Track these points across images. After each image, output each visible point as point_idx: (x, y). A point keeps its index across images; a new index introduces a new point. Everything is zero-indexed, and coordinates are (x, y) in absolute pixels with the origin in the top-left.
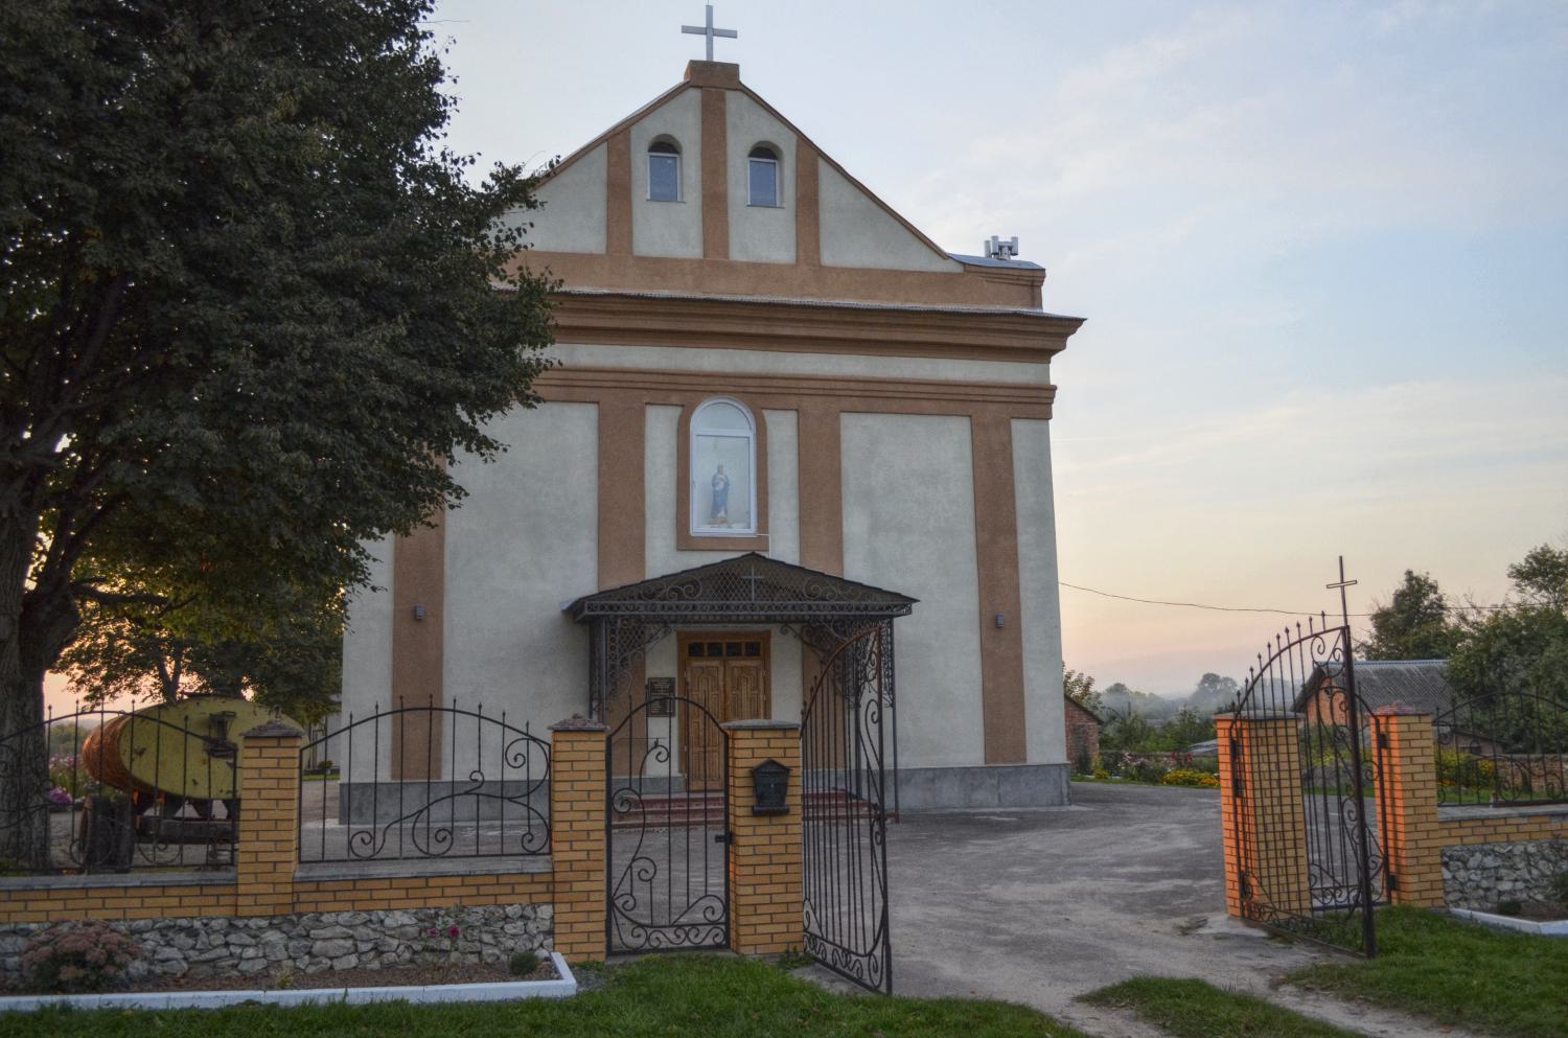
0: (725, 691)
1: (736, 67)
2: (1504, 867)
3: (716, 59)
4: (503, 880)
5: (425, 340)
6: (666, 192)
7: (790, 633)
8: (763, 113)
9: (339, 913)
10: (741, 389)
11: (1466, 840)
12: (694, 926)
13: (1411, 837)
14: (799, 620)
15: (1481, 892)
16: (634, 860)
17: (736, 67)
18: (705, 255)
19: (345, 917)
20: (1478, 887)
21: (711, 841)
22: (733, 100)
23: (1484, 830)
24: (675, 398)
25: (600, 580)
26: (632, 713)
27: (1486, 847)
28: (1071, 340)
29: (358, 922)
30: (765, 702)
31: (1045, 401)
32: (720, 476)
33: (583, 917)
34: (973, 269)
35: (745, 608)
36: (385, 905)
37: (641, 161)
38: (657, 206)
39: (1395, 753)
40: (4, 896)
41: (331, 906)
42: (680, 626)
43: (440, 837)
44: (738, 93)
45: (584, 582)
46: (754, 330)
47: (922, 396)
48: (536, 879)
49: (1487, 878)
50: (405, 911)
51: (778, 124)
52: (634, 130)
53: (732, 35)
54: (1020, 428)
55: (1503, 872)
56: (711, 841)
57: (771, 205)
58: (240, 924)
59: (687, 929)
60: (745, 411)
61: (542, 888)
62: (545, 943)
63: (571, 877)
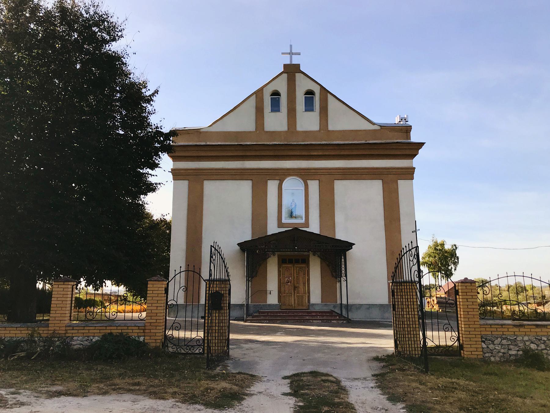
1: (300, 64)
2: (511, 344)
6: (276, 107)
7: (316, 255)
9: (78, 337)
12: (192, 346)
19: (80, 338)
20: (499, 352)
22: (298, 75)
24: (277, 178)
26: (175, 275)
27: (503, 336)
28: (420, 151)
29: (84, 340)
31: (412, 173)
32: (293, 203)
34: (384, 128)
41: (77, 335)
43: (113, 314)
44: (300, 74)
45: (247, 236)
46: (303, 154)
49: (504, 348)
52: (264, 89)
55: (511, 347)
57: (312, 110)
59: (190, 347)
60: (298, 179)
61: (142, 331)
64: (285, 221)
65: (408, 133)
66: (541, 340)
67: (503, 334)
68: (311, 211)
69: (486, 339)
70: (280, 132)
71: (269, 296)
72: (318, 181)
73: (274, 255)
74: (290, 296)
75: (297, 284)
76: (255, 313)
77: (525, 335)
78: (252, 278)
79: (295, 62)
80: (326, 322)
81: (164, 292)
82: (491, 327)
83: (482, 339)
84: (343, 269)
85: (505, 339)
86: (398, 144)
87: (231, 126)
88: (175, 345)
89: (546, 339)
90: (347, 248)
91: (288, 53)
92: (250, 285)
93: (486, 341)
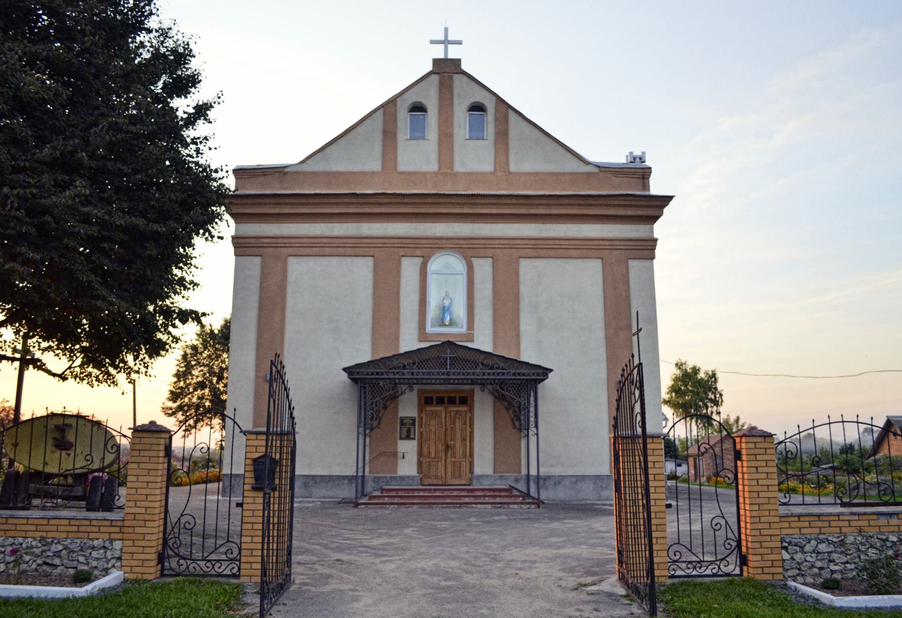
0: (446, 425)
1: (459, 60)
2: (835, 552)
5: (138, 202)
6: (418, 133)
7: (486, 390)
10: (457, 246)
11: (803, 531)
12: (218, 561)
13: (756, 526)
14: (493, 382)
15: (816, 570)
16: (182, 515)
17: (459, 60)
18: (440, 168)
20: (813, 566)
21: (233, 505)
23: (820, 524)
24: (418, 252)
25: (373, 355)
27: (821, 537)
29: (7, 544)
30: (470, 432)
33: (141, 550)
34: (604, 169)
35: (443, 374)
36: (23, 534)
37: (403, 116)
38: (412, 142)
39: (745, 464)
40: (4, 521)
42: (419, 386)
45: (365, 356)
48: (114, 523)
49: (821, 560)
51: (484, 92)
52: (399, 100)
53: (459, 43)
54: (634, 265)
55: (835, 556)
56: (233, 505)
59: (213, 563)
61: (117, 529)
62: (116, 565)
63: (135, 523)
65: (646, 180)
66: (887, 540)
67: (821, 533)
68: (477, 311)
70: (424, 174)
71: (400, 462)
72: (490, 261)
74: (438, 461)
75: (452, 440)
76: (375, 491)
78: (372, 429)
79: (452, 55)
80: (500, 507)
81: (162, 454)
82: (799, 521)
83: (782, 542)
84: (532, 414)
85: (824, 542)
86: (628, 198)
88: (184, 559)
89: (895, 539)
90: (538, 377)
93: (789, 547)
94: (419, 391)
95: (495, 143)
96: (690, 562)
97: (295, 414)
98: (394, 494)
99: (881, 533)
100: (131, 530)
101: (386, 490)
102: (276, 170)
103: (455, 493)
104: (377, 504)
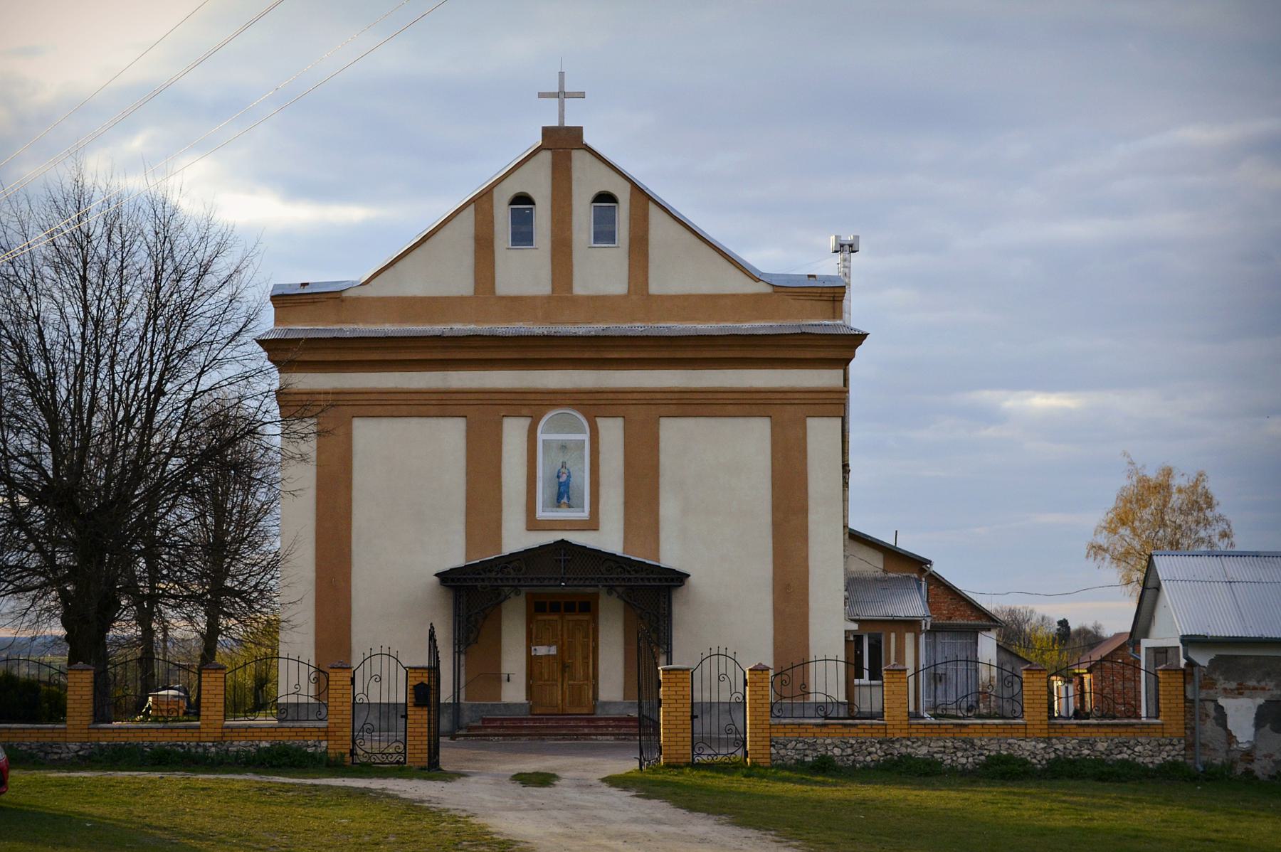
0: (562, 639)
1: (580, 129)
3: (567, 124)
4: (307, 730)
6: (523, 236)
8: (603, 166)
9: (240, 741)
10: (578, 402)
11: (787, 735)
17: (580, 129)
19: (242, 743)
22: (578, 157)
24: (525, 411)
25: (467, 559)
28: (858, 350)
30: (594, 648)
32: (563, 470)
34: (780, 290)
36: (258, 738)
41: (236, 739)
45: (456, 558)
46: (586, 356)
47: (728, 402)
49: (798, 754)
50: (267, 741)
52: (496, 190)
55: (808, 752)
58: (202, 744)
61: (323, 734)
64: (545, 514)
65: (837, 303)
66: (848, 742)
69: (777, 742)
70: (534, 298)
73: (518, 594)
74: (553, 685)
77: (827, 738)
81: (350, 683)
87: (413, 284)
89: (854, 742)
91: (554, 93)
92: (462, 662)
94: (527, 594)
95: (630, 252)
96: (710, 755)
97: (439, 655)
98: (498, 724)
99: (844, 738)
100: (333, 734)
101: (488, 719)
102: (330, 296)
103: (572, 723)
104: (478, 735)
